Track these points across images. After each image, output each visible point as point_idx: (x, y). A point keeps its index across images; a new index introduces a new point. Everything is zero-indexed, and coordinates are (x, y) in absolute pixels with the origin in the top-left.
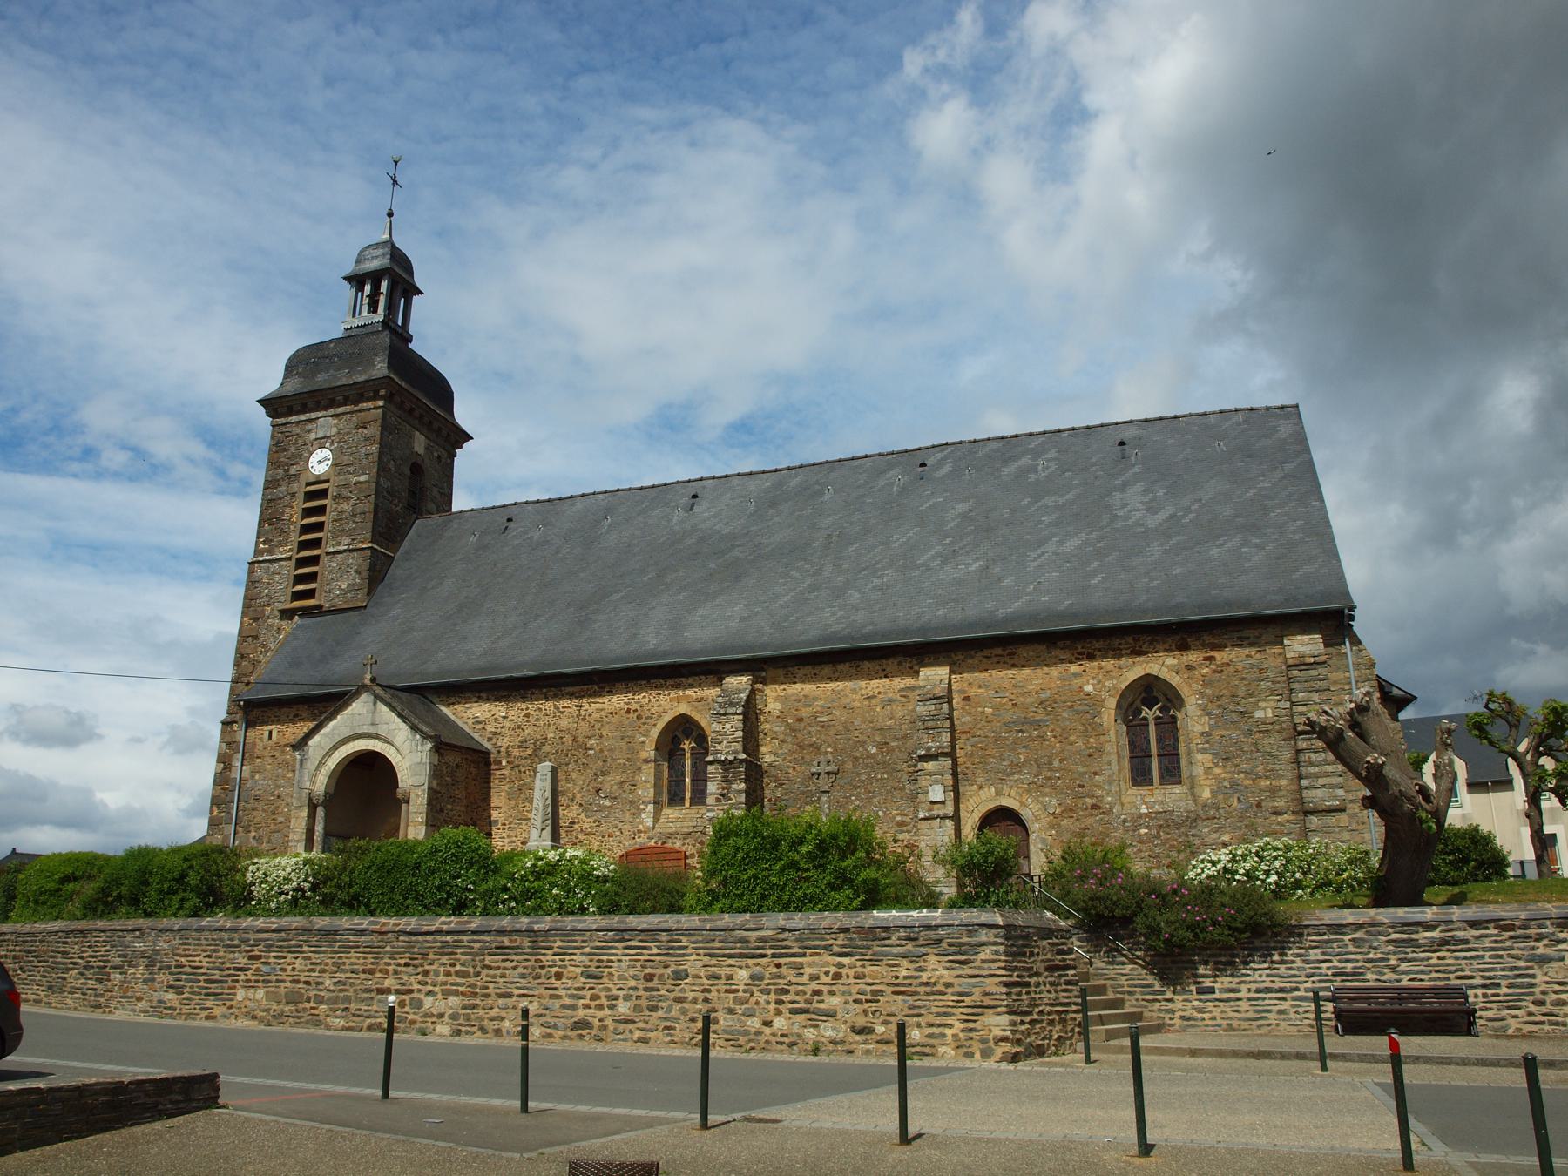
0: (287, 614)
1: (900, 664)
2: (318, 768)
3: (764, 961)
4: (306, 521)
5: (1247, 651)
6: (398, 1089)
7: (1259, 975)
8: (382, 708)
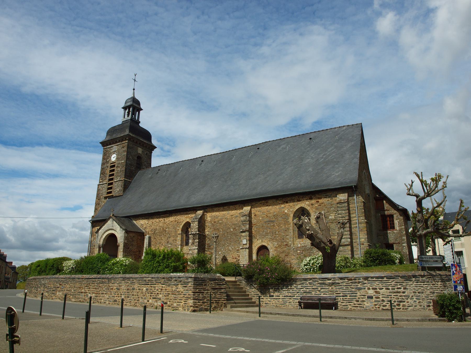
0: (106, 198)
5: (328, 199)
6: (96, 316)
7: (285, 292)
8: (114, 222)
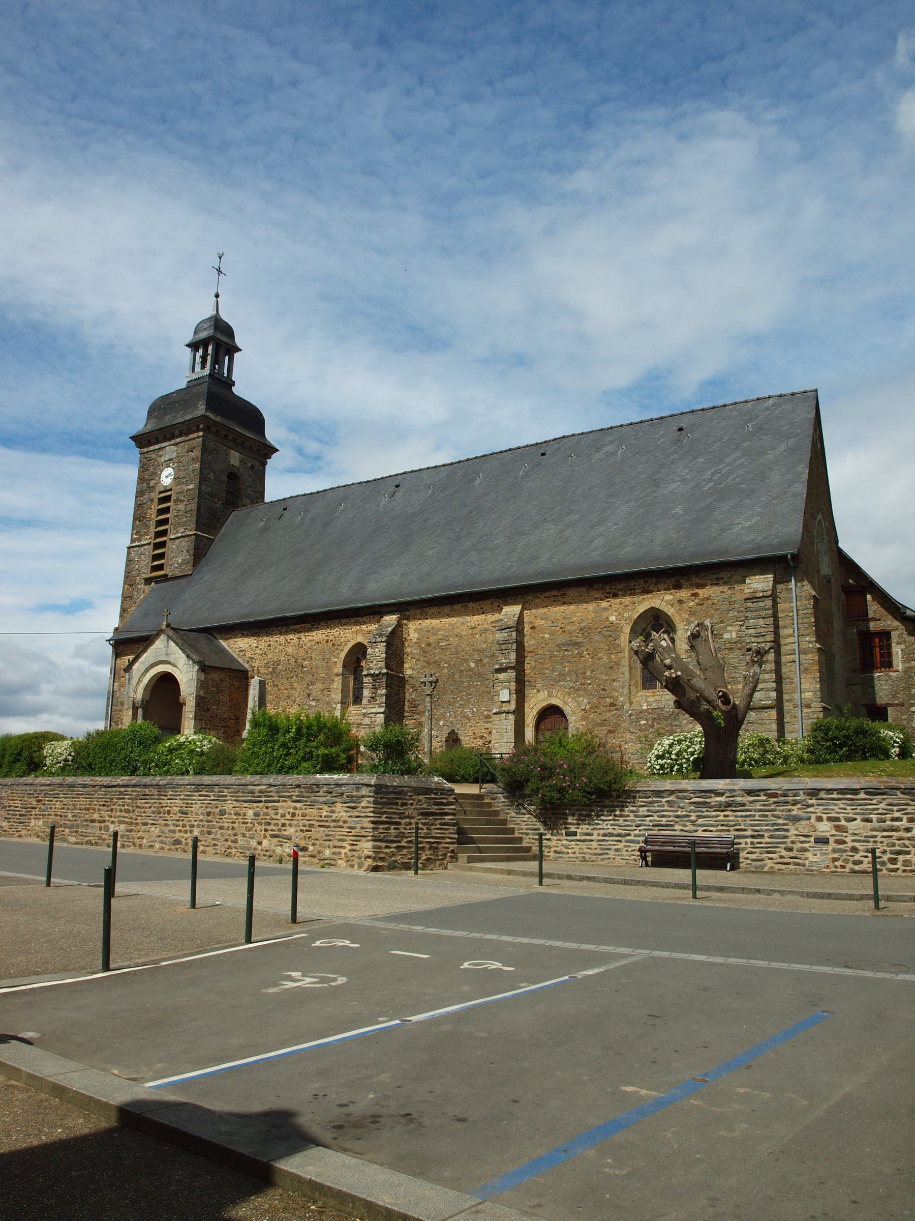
0: (148, 581)
1: (492, 604)
2: (138, 684)
3: (261, 805)
5: (721, 588)
7: (606, 824)
8: (172, 643)
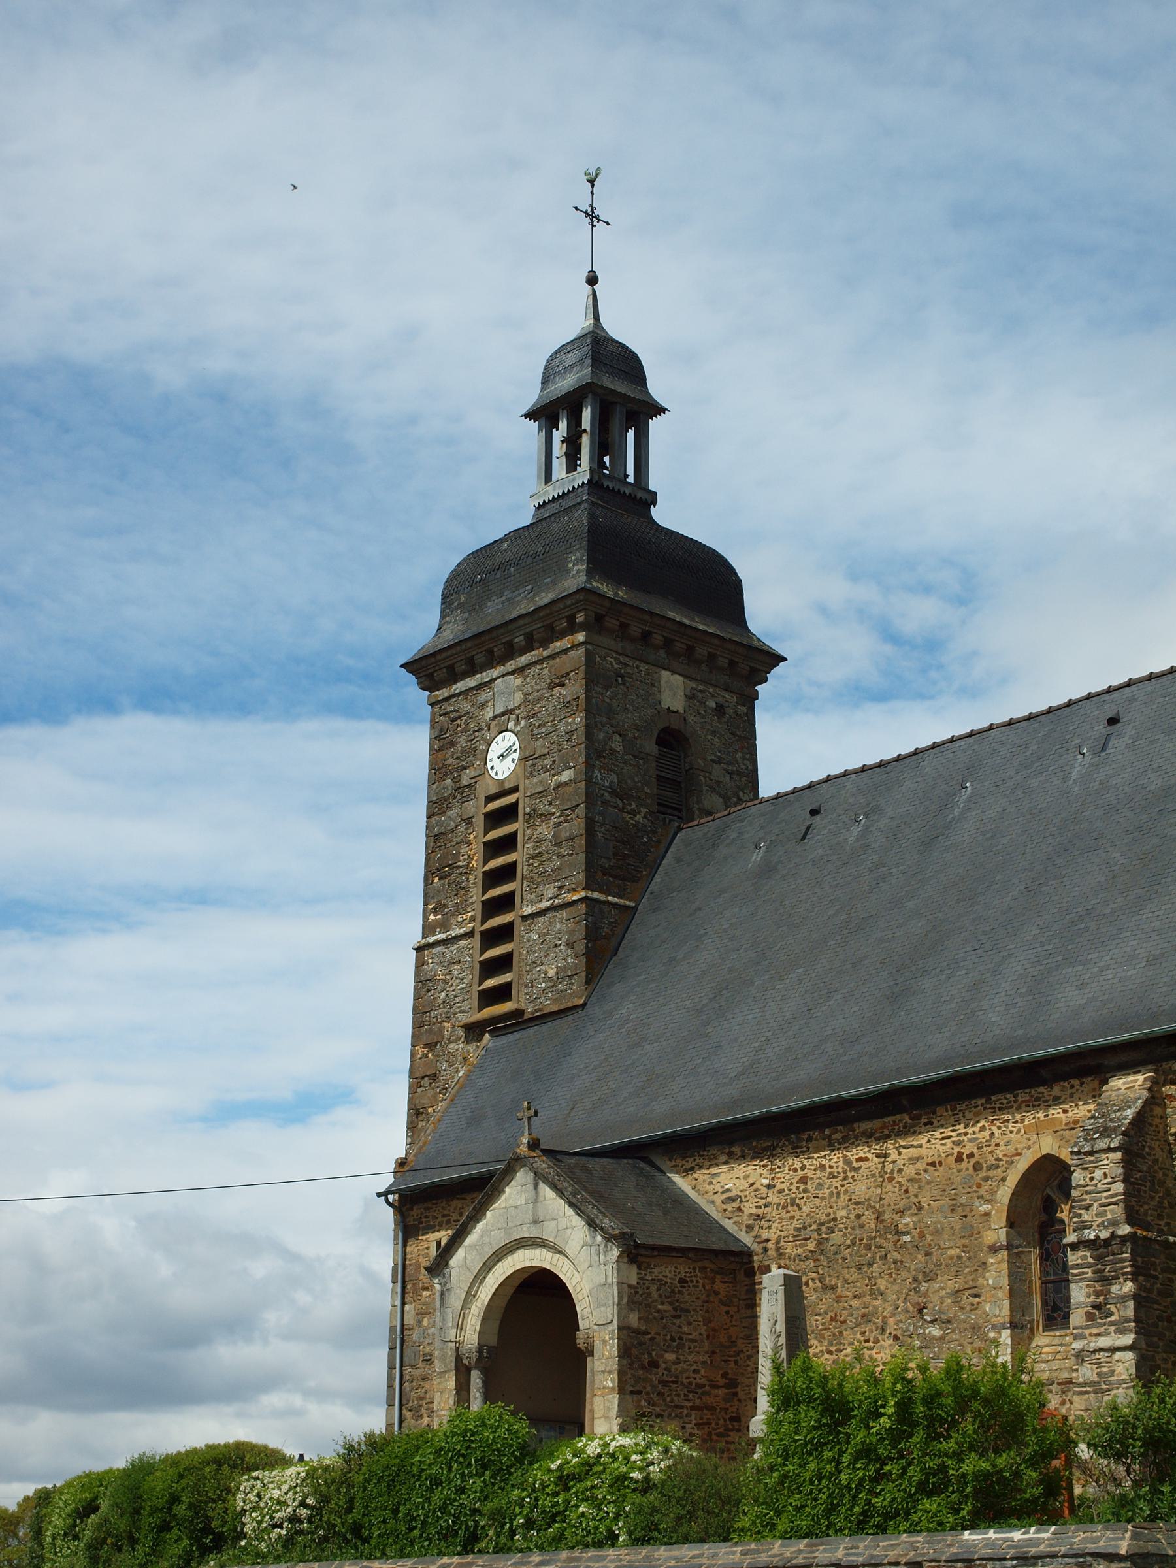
0: (474, 1031)
2: (466, 1304)
4: (494, 864)
8: (547, 1192)
